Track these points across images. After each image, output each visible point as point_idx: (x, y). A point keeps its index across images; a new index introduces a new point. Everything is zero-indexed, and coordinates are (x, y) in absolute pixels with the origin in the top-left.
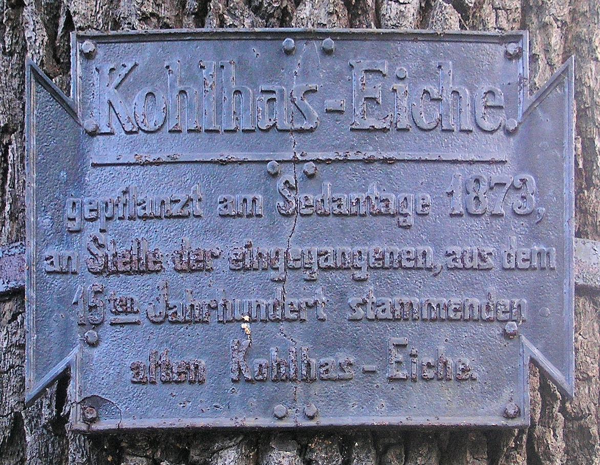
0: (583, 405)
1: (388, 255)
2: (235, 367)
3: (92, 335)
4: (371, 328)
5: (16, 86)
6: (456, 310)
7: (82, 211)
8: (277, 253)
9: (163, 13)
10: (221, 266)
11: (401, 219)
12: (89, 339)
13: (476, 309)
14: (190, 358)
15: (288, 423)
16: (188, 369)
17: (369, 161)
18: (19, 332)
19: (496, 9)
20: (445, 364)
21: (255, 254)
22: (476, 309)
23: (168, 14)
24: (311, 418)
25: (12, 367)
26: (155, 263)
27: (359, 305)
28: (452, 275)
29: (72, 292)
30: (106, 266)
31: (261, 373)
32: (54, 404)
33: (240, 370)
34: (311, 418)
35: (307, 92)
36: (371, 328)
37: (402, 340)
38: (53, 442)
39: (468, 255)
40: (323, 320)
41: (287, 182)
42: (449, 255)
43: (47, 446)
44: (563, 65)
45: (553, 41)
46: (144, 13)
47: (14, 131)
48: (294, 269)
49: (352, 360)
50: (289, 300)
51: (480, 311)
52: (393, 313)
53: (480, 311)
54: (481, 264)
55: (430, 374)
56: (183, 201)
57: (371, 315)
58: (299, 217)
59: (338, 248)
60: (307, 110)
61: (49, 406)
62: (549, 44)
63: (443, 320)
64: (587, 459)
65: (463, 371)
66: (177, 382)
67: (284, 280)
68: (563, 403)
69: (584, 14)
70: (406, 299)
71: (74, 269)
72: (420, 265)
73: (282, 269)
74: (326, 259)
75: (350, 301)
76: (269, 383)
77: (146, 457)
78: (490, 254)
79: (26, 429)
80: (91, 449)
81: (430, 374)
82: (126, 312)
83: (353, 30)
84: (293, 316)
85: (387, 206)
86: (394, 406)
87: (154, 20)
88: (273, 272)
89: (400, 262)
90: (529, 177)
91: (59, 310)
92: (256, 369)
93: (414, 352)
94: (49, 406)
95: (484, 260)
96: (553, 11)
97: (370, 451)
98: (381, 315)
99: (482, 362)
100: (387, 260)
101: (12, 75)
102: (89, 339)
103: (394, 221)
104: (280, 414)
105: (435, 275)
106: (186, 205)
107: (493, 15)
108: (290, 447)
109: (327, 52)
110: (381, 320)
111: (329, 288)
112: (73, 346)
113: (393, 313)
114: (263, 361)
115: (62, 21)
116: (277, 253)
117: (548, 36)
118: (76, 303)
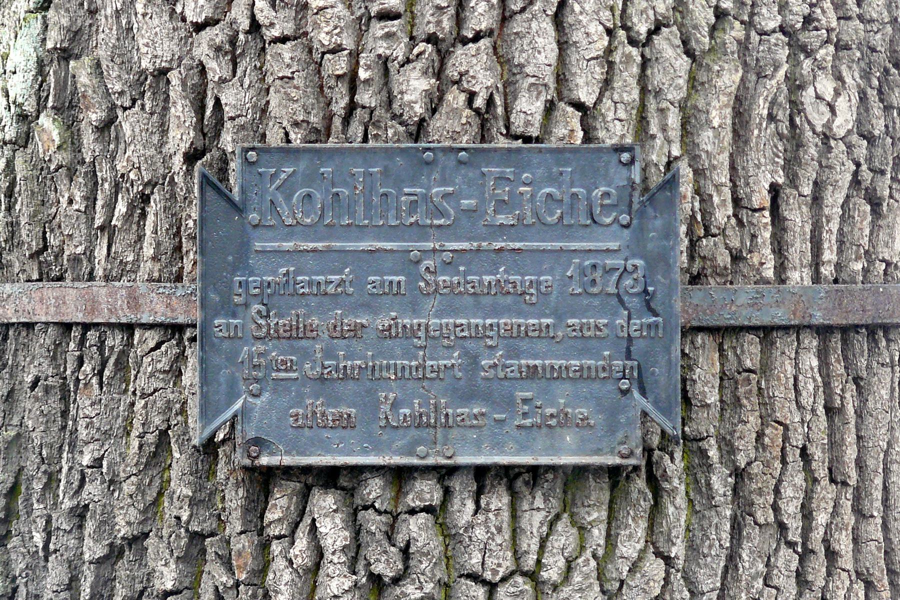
0: (702, 429)
1: (515, 327)
2: (382, 416)
3: (254, 387)
4: (501, 385)
5: (156, 142)
6: (575, 371)
7: (247, 289)
8: (419, 325)
9: (312, 119)
10: (370, 336)
11: (528, 297)
12: (254, 391)
13: (593, 370)
14: (345, 410)
15: (430, 461)
16: (341, 416)
18: (164, 359)
19: (616, 103)
21: (400, 326)
22: (593, 370)
23: (316, 120)
24: (450, 458)
26: (312, 331)
27: (490, 367)
28: (571, 342)
29: (237, 354)
30: (268, 333)
31: (405, 420)
33: (386, 418)
36: (501, 385)
37: (528, 394)
38: (202, 461)
39: (586, 327)
40: (460, 379)
41: (427, 268)
43: (197, 464)
45: (670, 122)
46: (295, 121)
48: (434, 338)
49: (484, 410)
50: (429, 363)
51: (597, 371)
52: (521, 373)
53: (597, 371)
54: (598, 333)
55: (553, 422)
57: (501, 375)
58: (438, 295)
59: (472, 321)
60: (446, 210)
62: (667, 125)
63: (564, 379)
64: (706, 477)
67: (426, 347)
69: (703, 84)
70: (531, 362)
71: (240, 335)
72: (543, 335)
73: (423, 339)
75: (483, 363)
76: (413, 428)
79: (174, 447)
81: (553, 422)
82: (286, 370)
83: (485, 146)
84: (434, 375)
85: (515, 287)
86: (522, 449)
87: (305, 125)
88: (416, 340)
89: (526, 332)
90: (639, 262)
91: (226, 368)
92: (401, 418)
93: (539, 404)
96: (670, 97)
97: (501, 479)
98: (510, 375)
99: (600, 412)
100: (515, 330)
101: (152, 132)
102: (254, 391)
103: (521, 299)
104: (423, 455)
106: (339, 285)
107: (613, 108)
108: (431, 477)
109: (461, 162)
110: (510, 379)
111: (465, 353)
113: (521, 373)
114: (407, 411)
115: (210, 103)
116: (419, 325)
117: (666, 118)
118: (242, 362)
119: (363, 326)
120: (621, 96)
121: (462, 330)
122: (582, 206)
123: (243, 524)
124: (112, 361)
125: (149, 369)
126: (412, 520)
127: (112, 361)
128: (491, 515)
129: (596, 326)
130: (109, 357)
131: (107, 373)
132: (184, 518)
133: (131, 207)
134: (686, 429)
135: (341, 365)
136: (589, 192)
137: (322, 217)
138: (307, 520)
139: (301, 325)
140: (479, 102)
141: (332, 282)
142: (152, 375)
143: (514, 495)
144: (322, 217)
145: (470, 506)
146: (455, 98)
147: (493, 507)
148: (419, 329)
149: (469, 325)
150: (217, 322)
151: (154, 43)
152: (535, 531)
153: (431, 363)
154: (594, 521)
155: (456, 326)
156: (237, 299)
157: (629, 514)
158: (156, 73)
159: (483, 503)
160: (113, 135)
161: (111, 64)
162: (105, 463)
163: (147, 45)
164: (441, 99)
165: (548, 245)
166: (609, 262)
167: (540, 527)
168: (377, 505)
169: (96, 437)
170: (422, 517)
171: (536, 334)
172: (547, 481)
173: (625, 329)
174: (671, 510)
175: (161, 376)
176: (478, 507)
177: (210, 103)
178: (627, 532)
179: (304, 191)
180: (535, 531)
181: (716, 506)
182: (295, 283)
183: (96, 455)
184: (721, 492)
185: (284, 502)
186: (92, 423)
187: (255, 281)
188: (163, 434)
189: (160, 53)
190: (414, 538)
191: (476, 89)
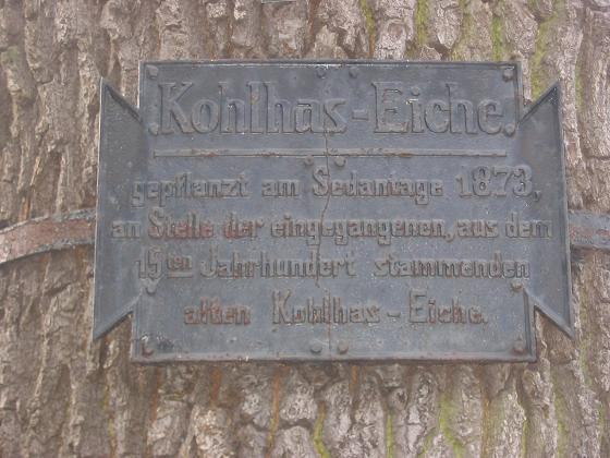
5: (69, 107)
17: (389, 156)
20: (460, 310)
25: (60, 328)
32: (98, 358)
34: (343, 353)
35: (336, 105)
42: (459, 226)
44: (69, 441)
47: (67, 143)
56: (233, 184)
61: (93, 360)
65: (475, 316)
66: (226, 323)
68: (549, 349)
74: (356, 230)
77: (183, 401)
78: (494, 225)
79: (72, 378)
80: (130, 395)
82: (182, 269)
90: (525, 167)
94: (93, 360)
95: (490, 230)
105: (449, 242)
112: (136, 294)
115: (112, 63)
119: (258, 226)
120: (477, 42)
121: (356, 230)
122: (470, 114)
123: (126, 447)
124: (27, 310)
125: (55, 309)
126: (287, 433)
127: (27, 310)
128: (366, 430)
129: (486, 225)
130: (26, 306)
131: (23, 318)
132: (76, 444)
133: (44, 165)
134: (552, 352)
135: (237, 262)
136: (475, 102)
137: (219, 124)
138: (189, 439)
139: (197, 227)
140: (349, 40)
141: (228, 185)
142: (56, 314)
143: (390, 409)
144: (219, 124)
145: (345, 420)
146: (326, 38)
147: (367, 421)
148: (313, 229)
149: (362, 224)
150: (116, 223)
151: (69, 19)
152: (411, 446)
153: (325, 261)
154: (469, 436)
155: (349, 225)
156: (135, 202)
157: (502, 429)
158: (69, 46)
159: (358, 417)
160: (35, 111)
161: (32, 48)
162: (18, 404)
163: (63, 22)
164: (314, 39)
165: (439, 151)
166: (498, 167)
167: (416, 443)
168: (255, 421)
169: (12, 380)
170: (296, 430)
171: (428, 233)
172: (422, 396)
173: (515, 230)
174: (544, 428)
175: (65, 315)
176: (353, 421)
177: (112, 63)
178: (502, 447)
179: (203, 101)
180: (411, 446)
181: (585, 426)
182: (192, 186)
183: (12, 397)
184: (590, 411)
185: (167, 422)
186: (9, 367)
187: (154, 185)
188: (64, 370)
189: (74, 27)
190: (289, 451)
191: (346, 27)
